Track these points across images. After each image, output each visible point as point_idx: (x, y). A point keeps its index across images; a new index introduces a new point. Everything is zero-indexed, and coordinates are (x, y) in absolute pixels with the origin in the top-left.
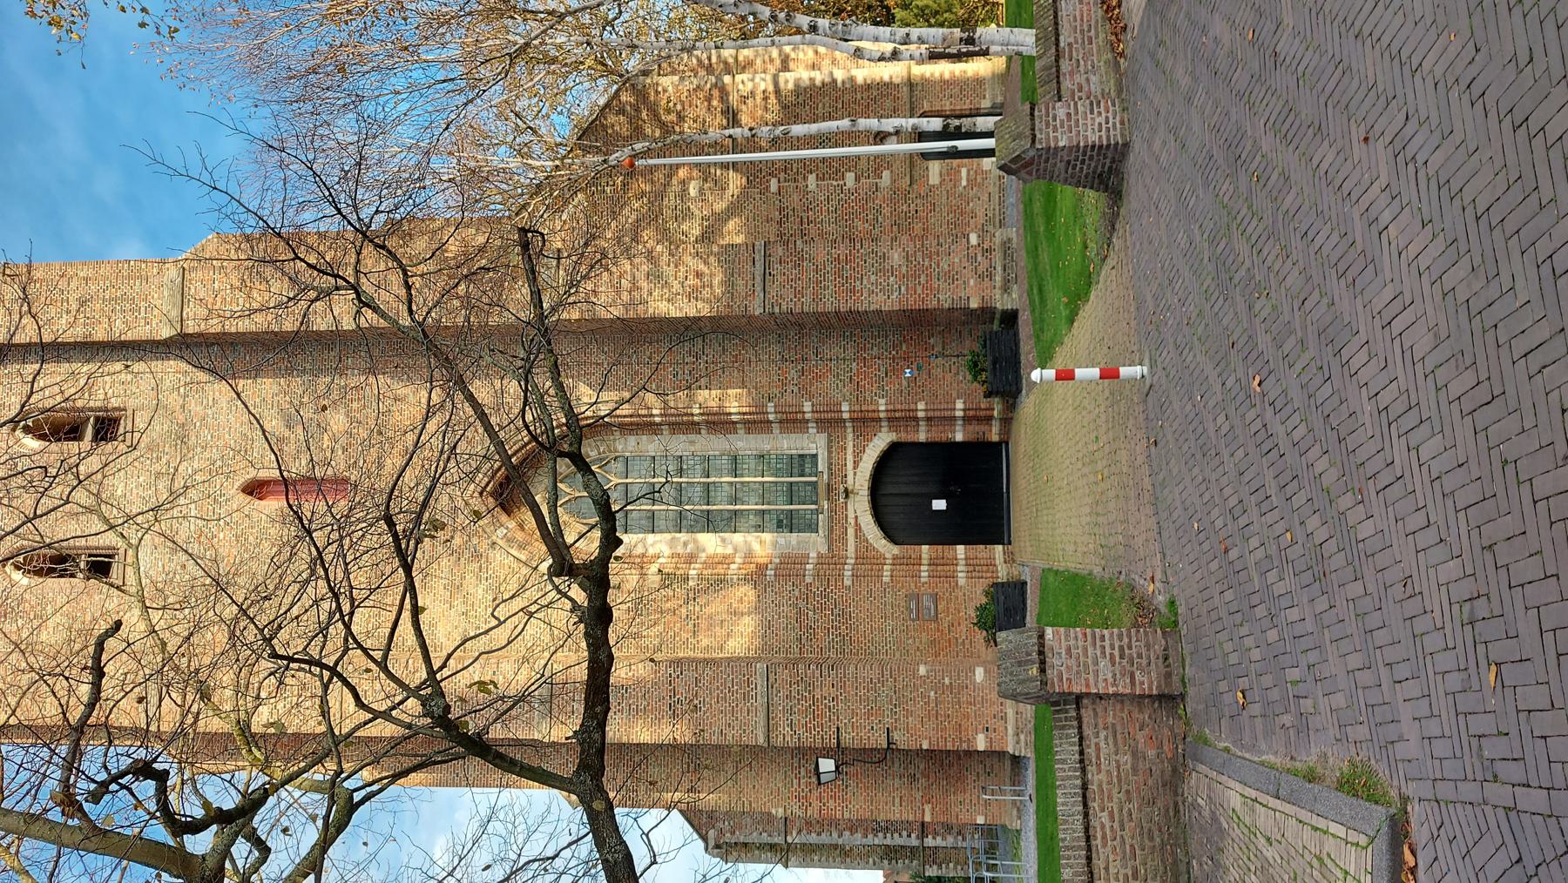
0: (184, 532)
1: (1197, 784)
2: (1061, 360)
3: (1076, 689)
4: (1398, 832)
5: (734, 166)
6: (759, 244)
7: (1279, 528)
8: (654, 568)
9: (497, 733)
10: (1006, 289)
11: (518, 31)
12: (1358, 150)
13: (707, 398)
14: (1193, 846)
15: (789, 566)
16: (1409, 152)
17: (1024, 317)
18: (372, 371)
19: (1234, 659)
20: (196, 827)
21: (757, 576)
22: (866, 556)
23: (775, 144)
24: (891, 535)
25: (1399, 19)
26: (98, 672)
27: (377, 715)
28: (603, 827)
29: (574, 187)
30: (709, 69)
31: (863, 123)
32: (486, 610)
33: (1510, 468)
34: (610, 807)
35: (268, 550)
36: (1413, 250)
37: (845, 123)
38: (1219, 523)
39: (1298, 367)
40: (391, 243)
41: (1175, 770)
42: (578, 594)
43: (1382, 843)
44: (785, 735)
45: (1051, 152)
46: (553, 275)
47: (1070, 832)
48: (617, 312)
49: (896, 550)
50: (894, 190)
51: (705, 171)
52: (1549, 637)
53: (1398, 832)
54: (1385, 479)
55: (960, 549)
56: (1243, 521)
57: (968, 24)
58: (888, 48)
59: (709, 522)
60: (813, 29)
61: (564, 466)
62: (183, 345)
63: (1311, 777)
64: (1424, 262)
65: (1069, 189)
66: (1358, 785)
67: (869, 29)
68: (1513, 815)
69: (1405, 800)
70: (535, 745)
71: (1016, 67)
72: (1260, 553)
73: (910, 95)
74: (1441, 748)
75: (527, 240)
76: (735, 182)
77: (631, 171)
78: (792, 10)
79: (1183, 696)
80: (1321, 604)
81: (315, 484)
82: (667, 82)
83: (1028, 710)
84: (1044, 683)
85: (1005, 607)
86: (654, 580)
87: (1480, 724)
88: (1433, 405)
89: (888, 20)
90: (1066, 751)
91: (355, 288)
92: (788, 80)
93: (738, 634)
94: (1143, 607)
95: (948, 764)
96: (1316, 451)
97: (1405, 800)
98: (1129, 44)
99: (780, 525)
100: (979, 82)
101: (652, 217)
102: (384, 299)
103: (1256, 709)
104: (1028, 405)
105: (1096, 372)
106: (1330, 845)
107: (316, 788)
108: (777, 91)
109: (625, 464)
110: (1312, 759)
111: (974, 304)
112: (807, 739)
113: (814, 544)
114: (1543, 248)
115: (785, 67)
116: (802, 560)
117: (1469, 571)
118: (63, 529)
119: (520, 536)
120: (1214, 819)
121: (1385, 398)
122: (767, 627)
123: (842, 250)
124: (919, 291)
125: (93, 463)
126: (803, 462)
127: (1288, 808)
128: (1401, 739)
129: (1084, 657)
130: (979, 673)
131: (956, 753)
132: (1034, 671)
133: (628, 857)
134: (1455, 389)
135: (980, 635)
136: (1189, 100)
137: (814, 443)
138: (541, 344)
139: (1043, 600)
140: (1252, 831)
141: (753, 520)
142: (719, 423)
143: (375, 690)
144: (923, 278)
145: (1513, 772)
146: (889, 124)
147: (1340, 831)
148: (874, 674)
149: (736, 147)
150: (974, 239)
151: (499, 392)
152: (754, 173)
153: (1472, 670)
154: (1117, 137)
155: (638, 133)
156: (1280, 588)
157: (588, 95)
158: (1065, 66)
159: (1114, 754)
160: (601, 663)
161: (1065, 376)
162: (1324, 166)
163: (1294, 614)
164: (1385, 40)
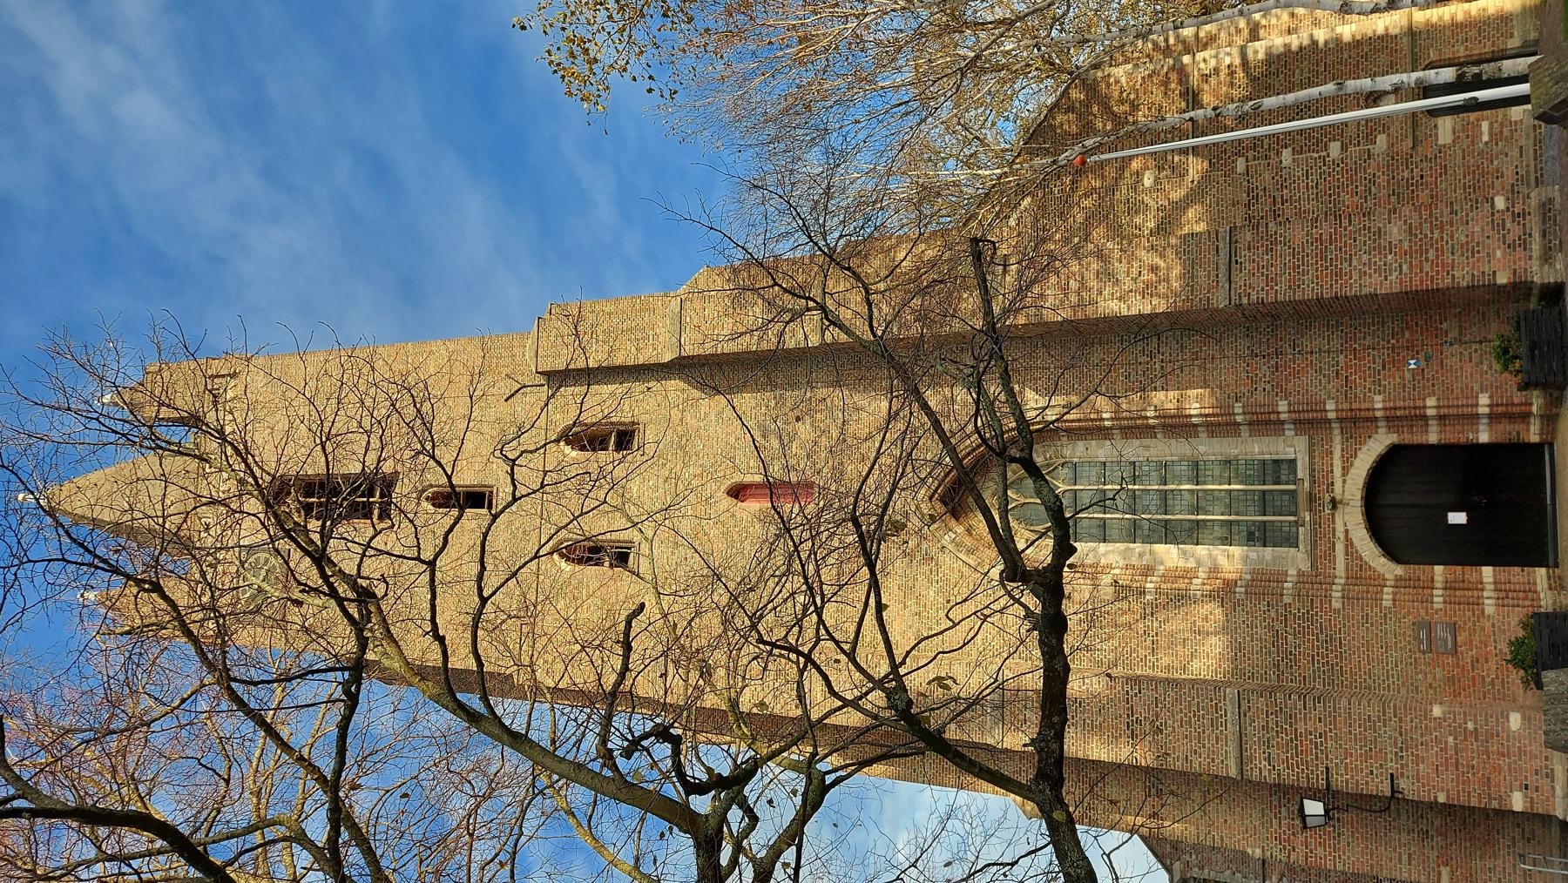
0: (685, 526)
5: (1195, 150)
6: (1224, 230)
8: (1106, 580)
9: (952, 733)
10: (1546, 258)
13: (1165, 399)
15: (1262, 585)
18: (838, 384)
20: (700, 789)
21: (1225, 593)
22: (1359, 575)
23: (1243, 121)
24: (1391, 551)
26: (628, 648)
27: (846, 703)
28: (1063, 838)
30: (1167, 51)
31: (1352, 85)
32: (944, 612)
34: (1071, 821)
37: (1329, 88)
40: (854, 263)
42: (1031, 601)
44: (1260, 769)
48: (1066, 314)
49: (1399, 570)
50: (1392, 155)
51: (1161, 161)
55: (1487, 572)
59: (1168, 533)
61: (1015, 471)
62: (684, 367)
75: (979, 251)
76: (1195, 168)
77: (1081, 169)
82: (1120, 72)
86: (1107, 592)
92: (1258, 50)
101: (1103, 215)
102: (845, 315)
107: (794, 766)
109: (1079, 469)
111: (1502, 279)
112: (1289, 777)
113: (1295, 560)
115: (1254, 35)
116: (1280, 577)
118: (598, 525)
119: (968, 541)
122: (1237, 651)
124: (1427, 267)
125: (619, 472)
126: (1278, 469)
130: (1515, 721)
131: (1485, 812)
135: (1516, 676)
137: (1293, 447)
138: (995, 350)
141: (1219, 532)
142: (1177, 426)
143: (846, 681)
144: (1431, 254)
146: (1386, 82)
148: (1373, 711)
149: (1197, 129)
150: (1500, 203)
151: (953, 400)
152: (1218, 157)
155: (1087, 129)
157: (1033, 97)
160: (1056, 672)
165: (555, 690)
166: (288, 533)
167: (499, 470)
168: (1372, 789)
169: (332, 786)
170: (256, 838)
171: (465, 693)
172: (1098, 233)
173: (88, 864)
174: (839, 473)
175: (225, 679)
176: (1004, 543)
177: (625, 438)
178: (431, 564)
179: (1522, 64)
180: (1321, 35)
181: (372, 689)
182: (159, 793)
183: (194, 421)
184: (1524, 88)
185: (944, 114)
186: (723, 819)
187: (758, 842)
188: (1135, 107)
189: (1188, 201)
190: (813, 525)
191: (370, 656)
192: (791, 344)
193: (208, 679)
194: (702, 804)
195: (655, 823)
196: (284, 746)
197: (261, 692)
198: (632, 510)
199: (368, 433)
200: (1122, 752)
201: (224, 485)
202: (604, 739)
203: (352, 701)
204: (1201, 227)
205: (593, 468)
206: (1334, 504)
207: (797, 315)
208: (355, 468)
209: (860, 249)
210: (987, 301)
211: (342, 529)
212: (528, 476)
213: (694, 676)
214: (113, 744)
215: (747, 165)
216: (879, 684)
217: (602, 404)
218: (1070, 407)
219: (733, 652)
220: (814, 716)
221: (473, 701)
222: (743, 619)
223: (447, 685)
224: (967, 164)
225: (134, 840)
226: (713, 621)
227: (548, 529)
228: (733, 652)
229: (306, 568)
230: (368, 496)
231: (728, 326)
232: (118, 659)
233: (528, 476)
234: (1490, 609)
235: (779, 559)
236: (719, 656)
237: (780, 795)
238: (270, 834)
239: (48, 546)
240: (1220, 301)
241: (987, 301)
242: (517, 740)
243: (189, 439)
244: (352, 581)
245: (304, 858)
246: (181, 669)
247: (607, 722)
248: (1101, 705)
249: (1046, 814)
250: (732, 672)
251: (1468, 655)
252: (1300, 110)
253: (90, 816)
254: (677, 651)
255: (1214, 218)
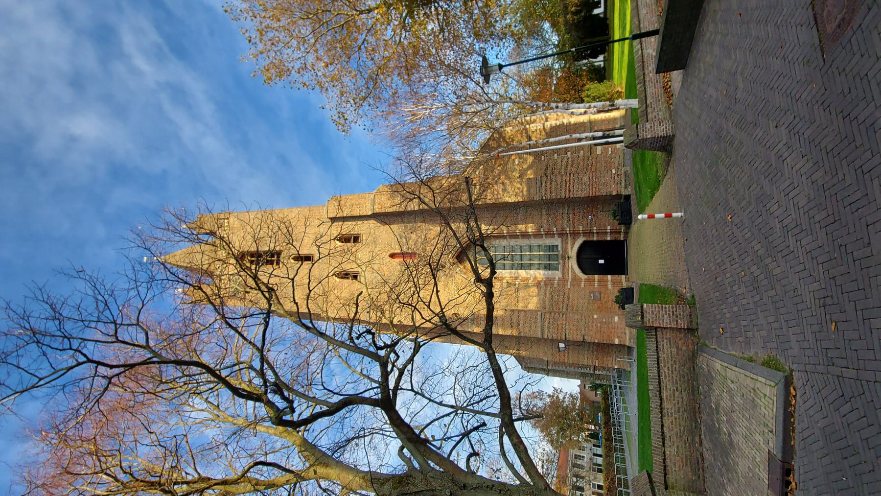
0: (376, 267)
1: (703, 360)
2: (649, 210)
3: (655, 325)
4: (788, 382)
5: (530, 153)
6: (538, 177)
7: (739, 270)
8: (504, 281)
9: (459, 328)
10: (626, 187)
11: (464, 119)
12: (772, 130)
13: (522, 227)
14: (701, 382)
15: (549, 282)
16: (796, 130)
17: (632, 197)
18: (424, 222)
19: (719, 317)
20: (381, 348)
21: (538, 284)
22: (575, 279)
23: (544, 145)
24: (584, 272)
25: (790, 81)
26: (357, 305)
27: (427, 321)
28: (492, 359)
29: (480, 164)
30: (522, 124)
31: (574, 136)
32: (457, 292)
33: (843, 249)
34: (494, 353)
35: (396, 273)
36: (798, 166)
37: (568, 136)
38: (713, 268)
39: (747, 211)
40: (429, 184)
41: (693, 355)
42: (484, 289)
43: (781, 385)
44: (547, 335)
45: (645, 140)
46: (476, 190)
47: (652, 373)
48: (494, 201)
49: (586, 277)
50: (584, 156)
51: (520, 156)
52: (859, 312)
53: (788, 382)
54: (786, 252)
55: (609, 277)
56: (723, 268)
57: (611, 99)
58: (583, 110)
59: (522, 267)
60: (557, 107)
61: (478, 249)
62: (375, 216)
63: (751, 360)
64: (803, 171)
65: (650, 153)
66: (770, 364)
67: (577, 105)
68: (841, 379)
69: (792, 371)
70: (469, 332)
71: (629, 112)
72: (731, 279)
73: (591, 126)
74: (808, 352)
75: (467, 181)
76: (530, 159)
77: (497, 158)
78: (549, 102)
79: (697, 329)
80: (757, 298)
81: (412, 255)
82: (508, 129)
83: (634, 331)
84: (643, 323)
85: (626, 297)
86: (505, 285)
87: (825, 344)
88: (808, 224)
89: (582, 101)
90: (651, 346)
91: (419, 198)
92: (548, 125)
93: (533, 304)
94: (681, 298)
95: (604, 348)
96: (755, 242)
97: (792, 371)
98: (674, 100)
99: (545, 268)
100: (615, 119)
101: (504, 172)
102: (426, 200)
103: (728, 335)
104: (634, 227)
105: (663, 215)
106: (758, 385)
107: (411, 340)
108: (544, 128)
109: (497, 248)
110: (751, 354)
111: (614, 194)
112: (555, 337)
113: (557, 274)
114: (858, 163)
115: (547, 120)
116: (554, 279)
117: (823, 286)
118: (349, 267)
119: (464, 270)
120: (709, 371)
121: (785, 222)
122: (542, 300)
123: (566, 178)
125: (354, 249)
126: (553, 248)
127: (741, 371)
128: (791, 348)
129: (658, 314)
130: (616, 319)
131: (608, 345)
132: (639, 318)
133: (500, 369)
134: (817, 218)
135: (616, 306)
136: (700, 118)
137: (557, 241)
138: (472, 212)
139: (640, 295)
140: (725, 378)
141: (537, 266)
142: (525, 235)
143: (426, 314)
145: (843, 363)
146: (583, 135)
147: (763, 380)
148: (578, 317)
149: (530, 147)
150: (614, 171)
151: (460, 227)
152: (536, 155)
153: (824, 324)
154: (670, 133)
155: (499, 146)
156: (738, 292)
157: (483, 136)
158: (649, 110)
159: (669, 349)
160: (490, 309)
161: (651, 217)
162: (758, 137)
163: (744, 302)
164: (784, 90)
165: (335, 319)
166: (244, 270)
167: (315, 249)
168: (577, 340)
169: (261, 351)
170: (237, 368)
171: (305, 320)
172: (502, 177)
173: (180, 378)
174: (424, 249)
175: (224, 317)
176: (475, 271)
177: (356, 239)
178: (293, 279)
179: (621, 132)
180: (565, 121)
181: (274, 320)
182: (204, 354)
183: (212, 233)
184: (621, 138)
185: (456, 139)
186: (389, 357)
187: (400, 363)
188: (513, 140)
189: (529, 168)
190: (416, 266)
191: (272, 308)
192: (409, 209)
193: (218, 318)
194: (382, 353)
195: (367, 359)
196: (245, 339)
197: (237, 321)
198: (359, 262)
199: (271, 237)
200: (509, 332)
201: (222, 254)
202: (350, 334)
203: (267, 324)
204: (532, 176)
205: (346, 248)
206: (569, 258)
207: (411, 200)
208: (267, 249)
209: (431, 180)
210: (470, 197)
211: (261, 269)
212: (324, 251)
213: (379, 314)
214: (187, 339)
215: (396, 152)
216: (437, 315)
217: (349, 228)
218: (494, 229)
219: (391, 305)
220: (417, 325)
221: (307, 322)
222: (394, 297)
223: (299, 318)
224: (463, 155)
225: (194, 369)
226: (385, 297)
227: (331, 268)
228: (391, 305)
229: (251, 282)
230: (273, 257)
231: (389, 203)
232: (187, 311)
233: (324, 251)
234: (610, 286)
235: (406, 277)
236: (387, 307)
237: (406, 349)
238: (242, 366)
239: (161, 274)
240: (537, 198)
241: (470, 197)
242: (322, 335)
243: (211, 239)
244: (266, 285)
245: (253, 374)
246: (209, 315)
247: (351, 329)
248: (502, 318)
249: (486, 351)
250: (391, 312)
251: (604, 300)
252: (559, 143)
253: (179, 363)
254: (374, 306)
255: (535, 174)
